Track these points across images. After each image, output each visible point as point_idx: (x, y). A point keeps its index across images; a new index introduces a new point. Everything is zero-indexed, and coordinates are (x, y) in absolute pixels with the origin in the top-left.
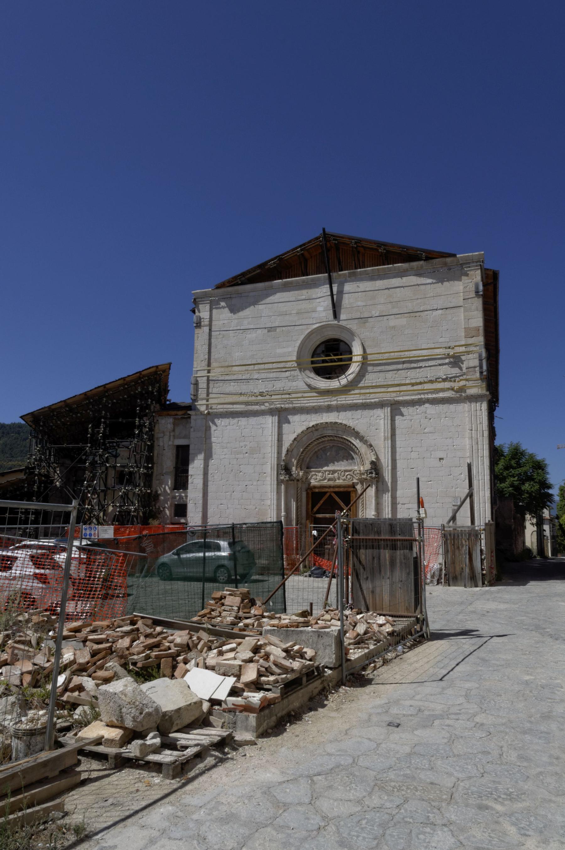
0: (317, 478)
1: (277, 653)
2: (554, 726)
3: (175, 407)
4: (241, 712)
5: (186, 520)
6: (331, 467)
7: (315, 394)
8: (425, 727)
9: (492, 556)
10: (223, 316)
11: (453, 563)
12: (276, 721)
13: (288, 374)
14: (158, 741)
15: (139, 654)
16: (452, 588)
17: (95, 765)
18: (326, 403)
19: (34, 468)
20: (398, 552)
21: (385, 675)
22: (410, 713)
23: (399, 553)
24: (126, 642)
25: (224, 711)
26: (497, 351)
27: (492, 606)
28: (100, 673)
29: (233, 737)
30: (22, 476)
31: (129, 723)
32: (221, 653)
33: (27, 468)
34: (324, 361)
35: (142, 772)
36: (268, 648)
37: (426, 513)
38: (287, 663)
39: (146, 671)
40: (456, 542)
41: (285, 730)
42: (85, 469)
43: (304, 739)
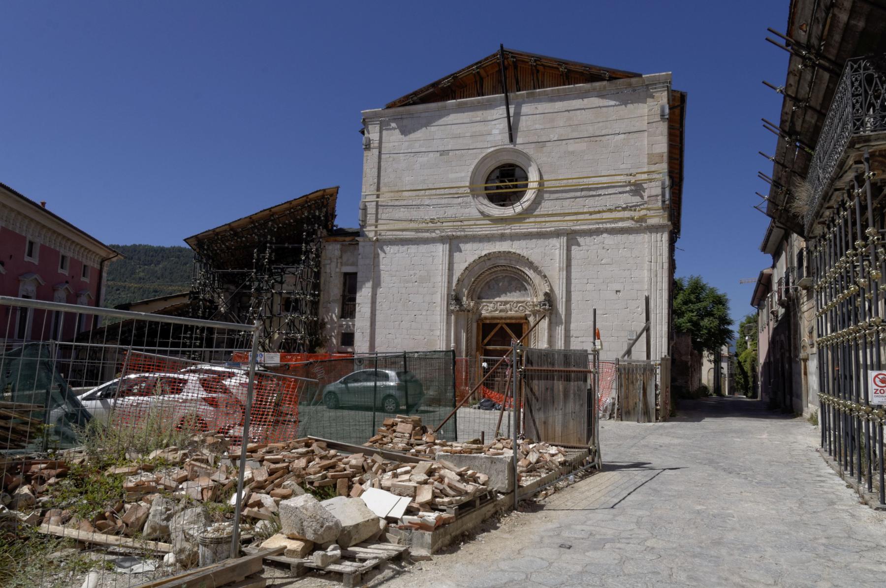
0: (489, 309)
1: (451, 476)
2: (724, 551)
3: (342, 233)
4: (417, 529)
5: (354, 349)
6: (503, 298)
7: (488, 222)
8: (595, 549)
9: (667, 392)
10: (393, 138)
11: (627, 397)
12: (451, 539)
13: (460, 200)
14: (338, 552)
15: (315, 474)
16: (625, 423)
17: (278, 573)
18: (500, 232)
19: (198, 293)
20: (572, 383)
21: (556, 502)
22: (581, 536)
23: (573, 385)
24: (302, 462)
25: (400, 528)
26: (681, 179)
27: (666, 440)
28: (278, 491)
29: (409, 553)
30: (186, 301)
31: (310, 536)
32: (395, 476)
33: (192, 292)
34: (498, 188)
35: (323, 580)
36: (442, 472)
37: (601, 345)
38: (462, 486)
39: (323, 490)
40: (630, 376)
41: (459, 548)
42: (249, 296)
43: (478, 557)
